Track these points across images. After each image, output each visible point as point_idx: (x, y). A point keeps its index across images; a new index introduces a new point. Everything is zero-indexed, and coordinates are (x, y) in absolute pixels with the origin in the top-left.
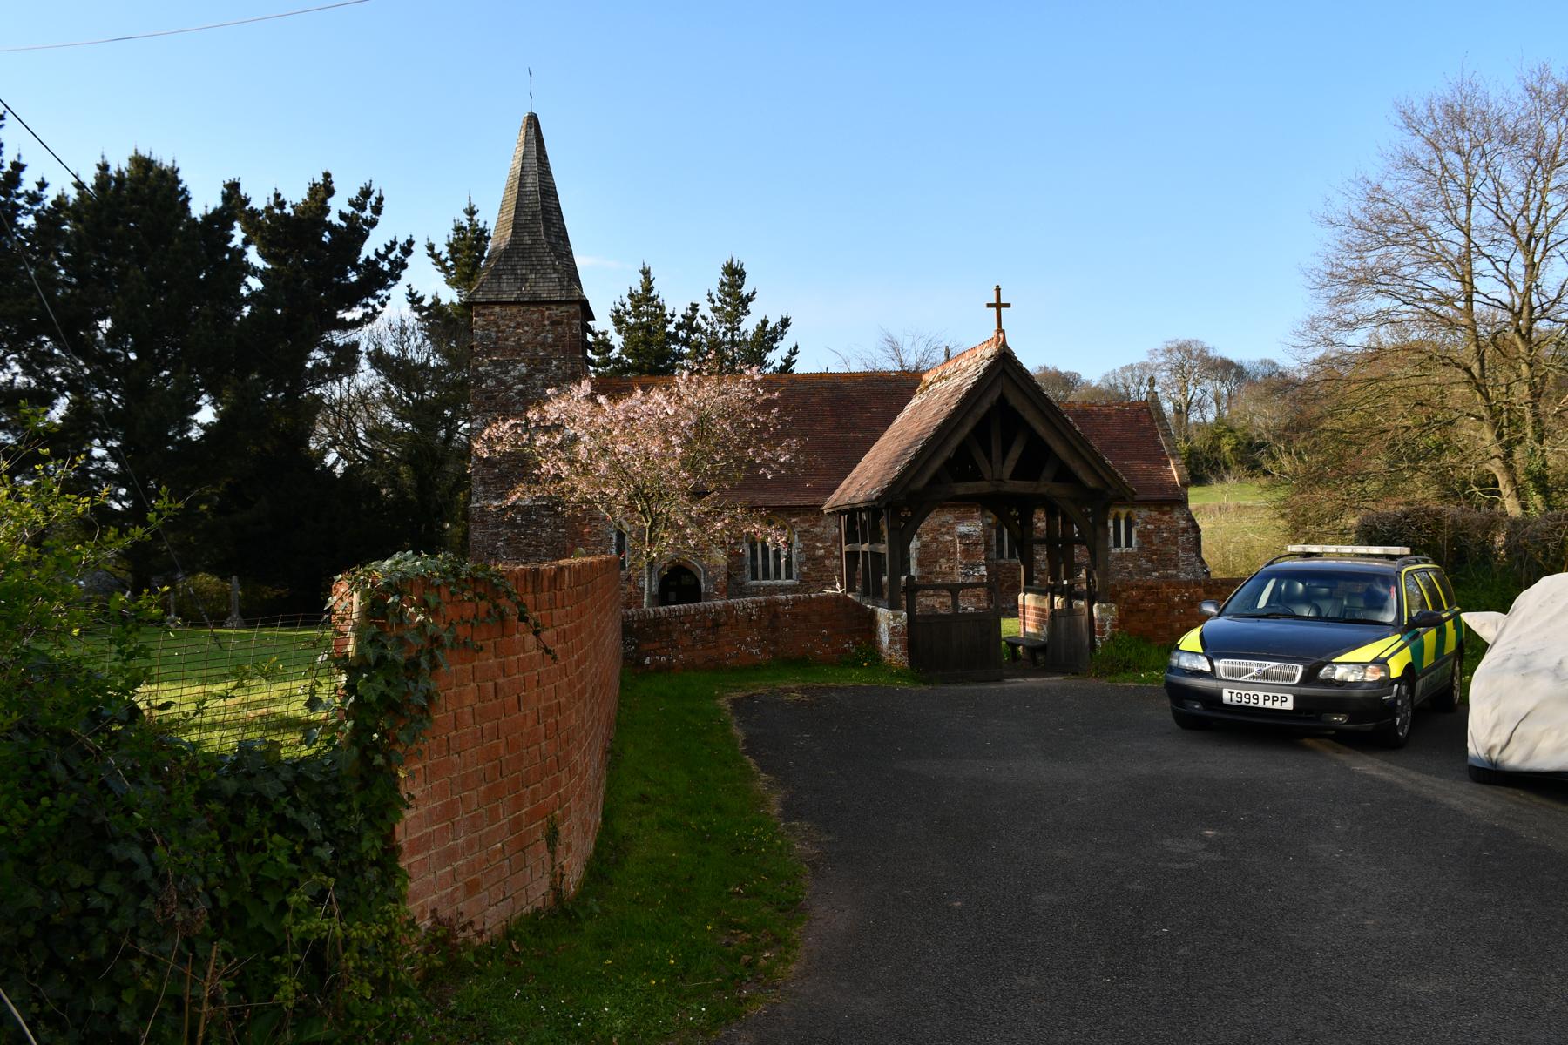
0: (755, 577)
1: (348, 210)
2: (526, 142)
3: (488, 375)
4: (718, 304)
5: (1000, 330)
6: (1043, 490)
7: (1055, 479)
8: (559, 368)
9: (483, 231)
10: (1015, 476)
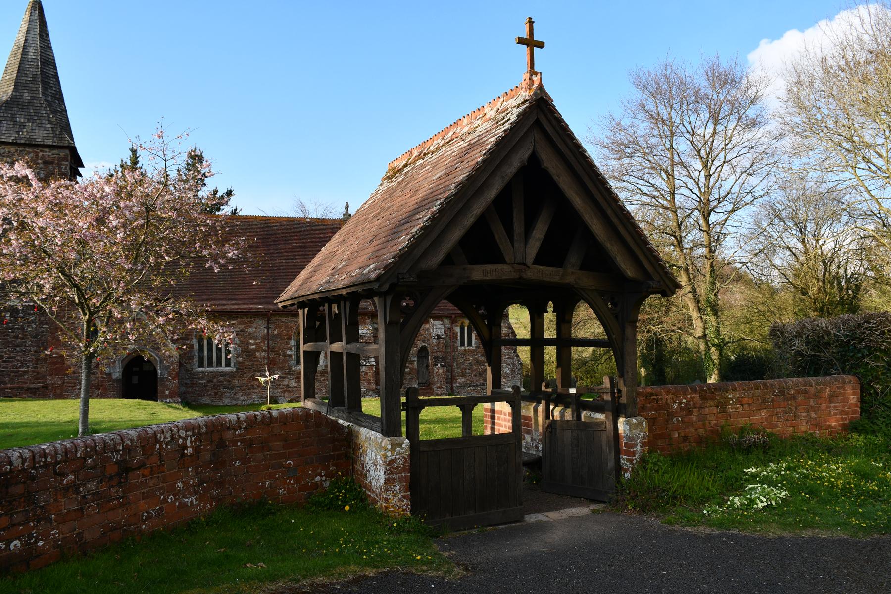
0: (201, 365)
2: (30, 21)
5: (532, 72)
6: (570, 279)
7: (583, 267)
10: (539, 260)
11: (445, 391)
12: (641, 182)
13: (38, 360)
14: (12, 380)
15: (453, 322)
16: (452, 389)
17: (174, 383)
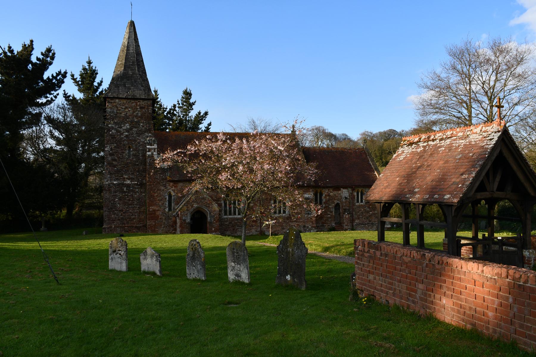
0: (226, 214)
1: (41, 57)
2: (130, 32)
3: (113, 128)
4: (181, 105)
8: (143, 126)
9: (94, 71)
11: (349, 227)
12: (453, 110)
13: (140, 212)
14: (128, 223)
15: (353, 190)
16: (353, 226)
17: (216, 225)
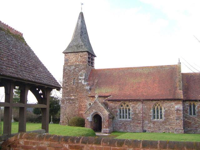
0: (120, 118)
